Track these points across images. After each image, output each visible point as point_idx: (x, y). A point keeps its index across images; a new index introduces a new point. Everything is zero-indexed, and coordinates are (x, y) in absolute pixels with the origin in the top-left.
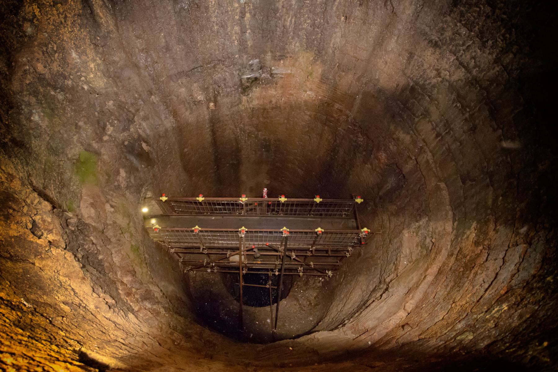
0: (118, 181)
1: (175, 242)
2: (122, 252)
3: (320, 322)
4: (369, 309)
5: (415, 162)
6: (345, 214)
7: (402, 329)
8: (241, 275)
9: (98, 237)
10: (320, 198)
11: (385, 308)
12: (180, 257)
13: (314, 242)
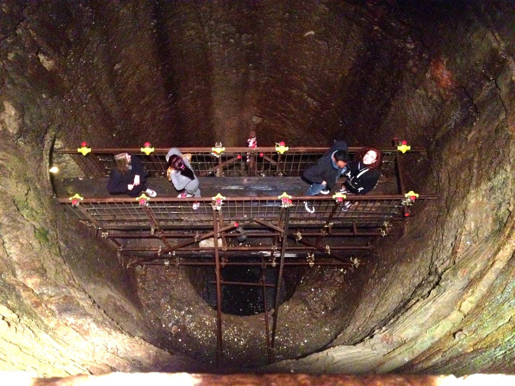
1: (110, 221)
2: (21, 240)
3: (340, 333)
5: (494, 85)
7: (453, 338)
8: (218, 267)
10: (144, 153)
11: (433, 310)
13: (331, 216)
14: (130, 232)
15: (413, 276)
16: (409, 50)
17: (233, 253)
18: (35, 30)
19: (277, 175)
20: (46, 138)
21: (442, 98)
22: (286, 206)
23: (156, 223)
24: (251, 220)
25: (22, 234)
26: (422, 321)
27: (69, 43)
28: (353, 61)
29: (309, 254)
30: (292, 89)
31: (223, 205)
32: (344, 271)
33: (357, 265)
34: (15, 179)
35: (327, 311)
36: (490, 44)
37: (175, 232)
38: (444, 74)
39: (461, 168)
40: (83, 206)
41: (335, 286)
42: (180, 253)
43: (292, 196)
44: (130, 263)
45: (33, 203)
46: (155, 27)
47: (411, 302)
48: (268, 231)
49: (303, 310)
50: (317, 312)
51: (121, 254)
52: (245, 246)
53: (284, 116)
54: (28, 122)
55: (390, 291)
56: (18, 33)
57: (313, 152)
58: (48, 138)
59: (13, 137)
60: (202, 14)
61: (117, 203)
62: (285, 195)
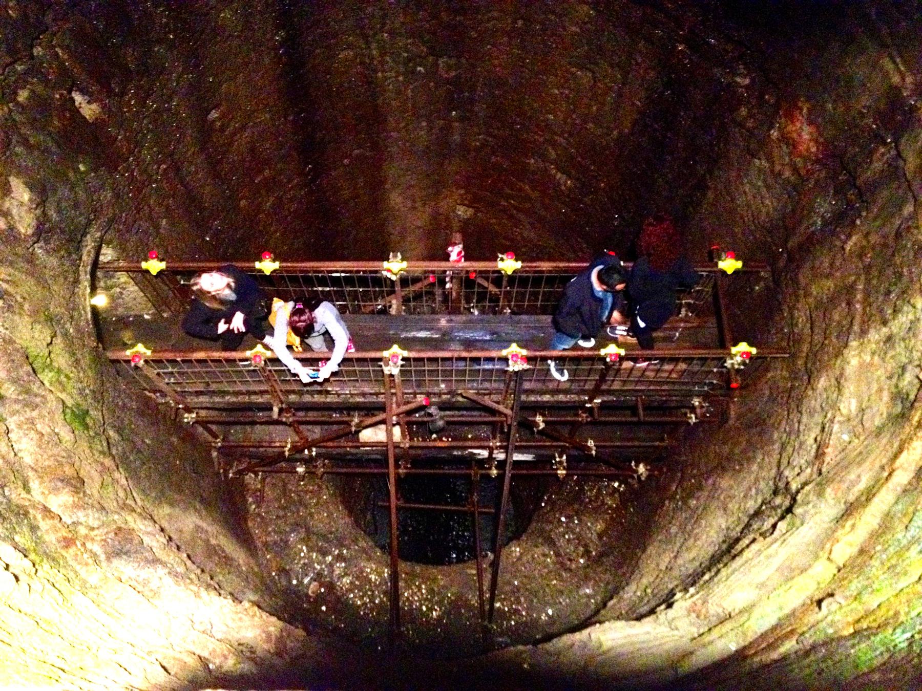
1: (198, 393)
3: (611, 598)
4: (739, 561)
5: (893, 152)
6: (688, 305)
7: (817, 609)
10: (260, 271)
12: (215, 436)
15: (745, 496)
19: (501, 312)
27: (127, 75)
31: (402, 366)
32: (620, 486)
33: (644, 475)
34: (30, 316)
35: (589, 557)
36: (886, 75)
37: (315, 414)
39: (833, 300)
42: (324, 450)
45: (62, 360)
47: (741, 543)
49: (544, 555)
50: (570, 560)
53: (513, 206)
54: (53, 214)
56: (35, 54)
58: (89, 244)
61: (212, 361)
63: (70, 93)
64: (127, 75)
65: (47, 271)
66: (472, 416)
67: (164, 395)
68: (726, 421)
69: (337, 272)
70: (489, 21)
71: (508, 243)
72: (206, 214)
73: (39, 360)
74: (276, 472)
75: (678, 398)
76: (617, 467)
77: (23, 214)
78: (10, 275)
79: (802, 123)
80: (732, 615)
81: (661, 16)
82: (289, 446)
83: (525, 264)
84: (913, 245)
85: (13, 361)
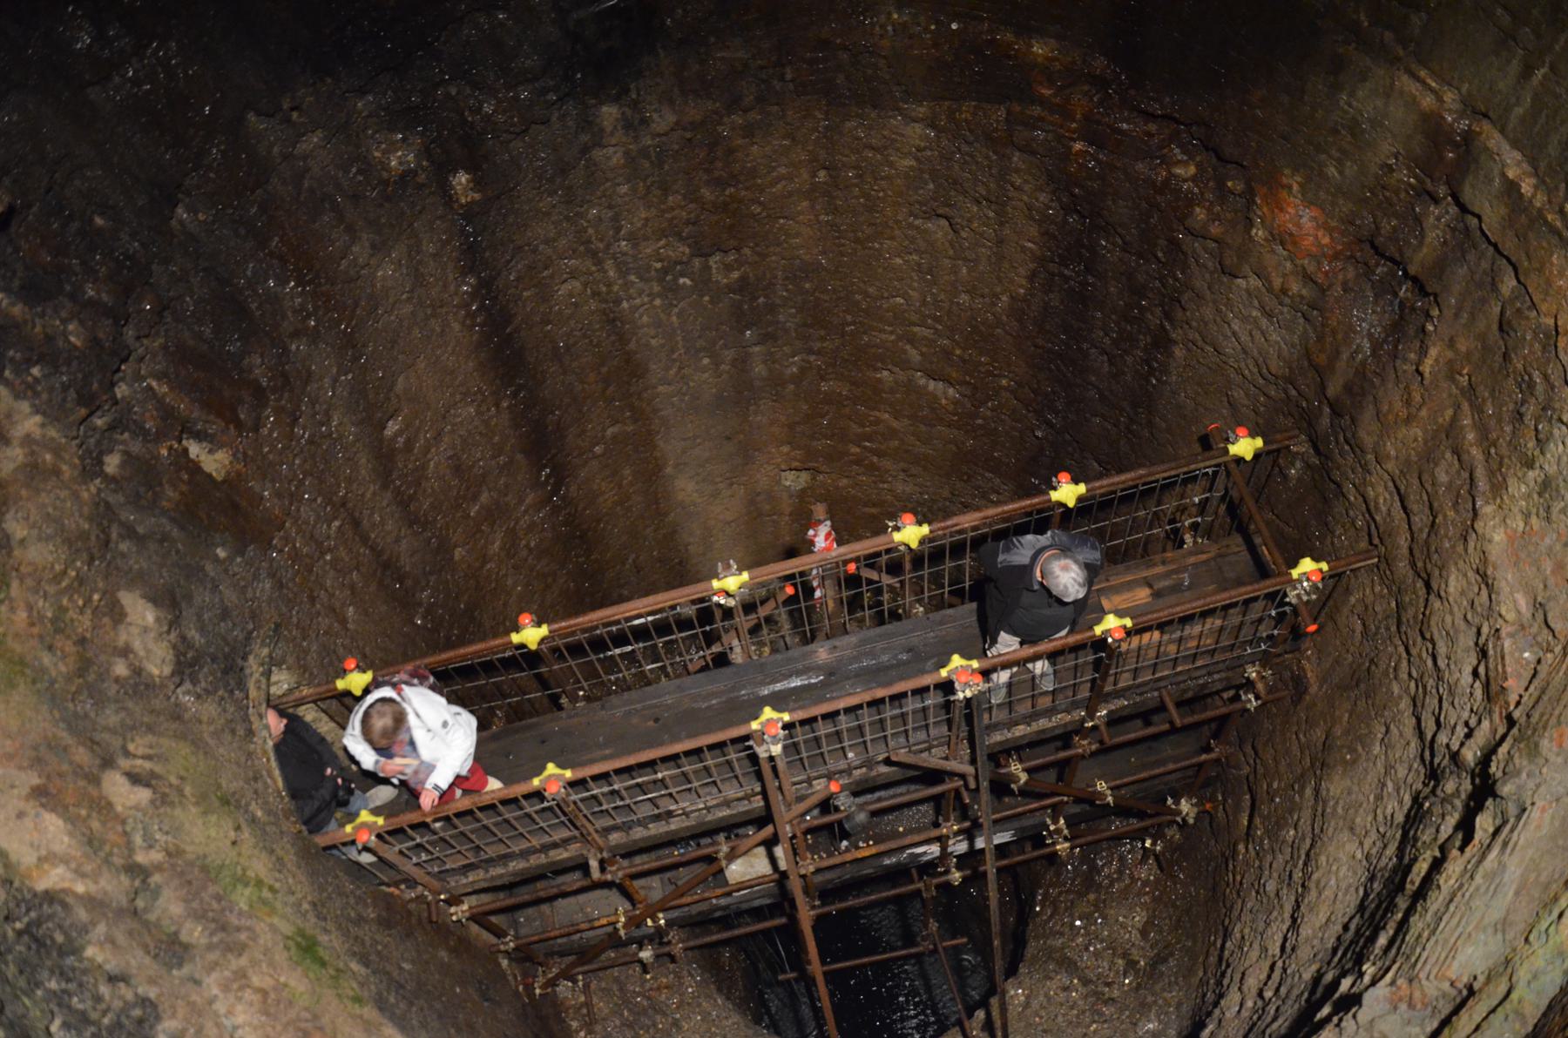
0: (126, 652)
4: (1435, 901)
5: (1453, 210)
9: (121, 939)
10: (522, 646)
14: (515, 891)
15: (1379, 798)
16: (1185, 180)
17: (829, 875)
18: (159, 377)
19: (908, 615)
20: (247, 671)
21: (1315, 283)
22: (968, 694)
23: (600, 841)
24: (869, 764)
25: (254, 963)
26: (1496, 914)
27: (260, 394)
28: (1032, 251)
29: (1049, 821)
30: (876, 370)
32: (1154, 844)
33: (1192, 815)
34: (197, 804)
35: (1137, 972)
36: (1413, 102)
37: (645, 857)
38: (1303, 218)
39: (1429, 457)
40: (386, 842)
41: (1139, 895)
42: (675, 914)
43: (790, 711)
44: (541, 980)
45: (260, 866)
46: (474, 295)
47: (1415, 869)
48: (913, 787)
49: (1066, 989)
50: (1108, 985)
51: (510, 959)
52: (857, 848)
53: (870, 450)
54: (193, 634)
55: (1323, 859)
56: (119, 396)
57: (1005, 520)
58: (253, 667)
59: (163, 686)
60: (591, 231)
61: (481, 809)
62: (957, 661)
63: (180, 442)
64: (260, 394)
65: (204, 727)
66: (901, 794)
67: (411, 883)
68: (1306, 690)
69: (639, 616)
70: (772, 184)
71: (874, 511)
72: (409, 583)
73: (225, 872)
74: (606, 968)
75: (1223, 675)
76: (1141, 815)
77: (151, 645)
78: (151, 747)
79: (1296, 206)
80: (1476, 986)
81: (1037, 110)
82: (623, 919)
83: (936, 525)
84: (1536, 334)
85: (190, 883)
